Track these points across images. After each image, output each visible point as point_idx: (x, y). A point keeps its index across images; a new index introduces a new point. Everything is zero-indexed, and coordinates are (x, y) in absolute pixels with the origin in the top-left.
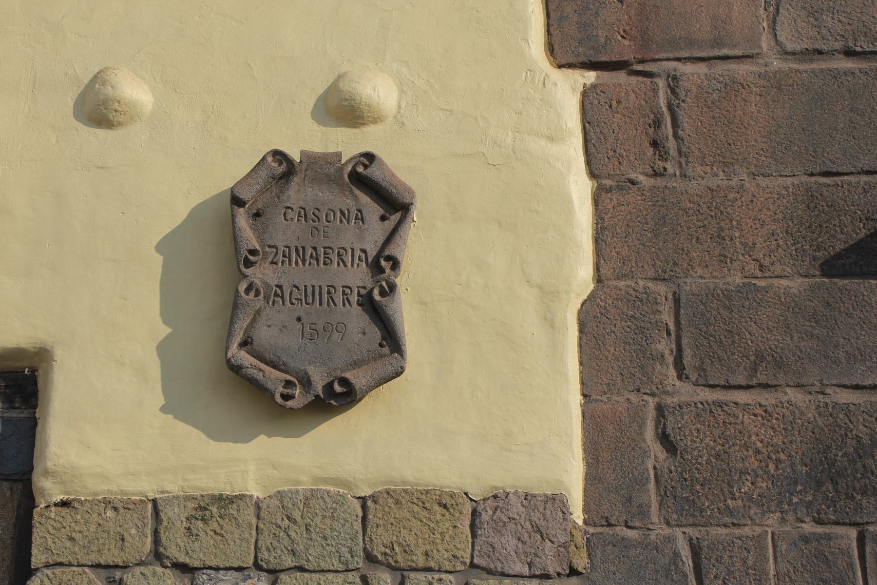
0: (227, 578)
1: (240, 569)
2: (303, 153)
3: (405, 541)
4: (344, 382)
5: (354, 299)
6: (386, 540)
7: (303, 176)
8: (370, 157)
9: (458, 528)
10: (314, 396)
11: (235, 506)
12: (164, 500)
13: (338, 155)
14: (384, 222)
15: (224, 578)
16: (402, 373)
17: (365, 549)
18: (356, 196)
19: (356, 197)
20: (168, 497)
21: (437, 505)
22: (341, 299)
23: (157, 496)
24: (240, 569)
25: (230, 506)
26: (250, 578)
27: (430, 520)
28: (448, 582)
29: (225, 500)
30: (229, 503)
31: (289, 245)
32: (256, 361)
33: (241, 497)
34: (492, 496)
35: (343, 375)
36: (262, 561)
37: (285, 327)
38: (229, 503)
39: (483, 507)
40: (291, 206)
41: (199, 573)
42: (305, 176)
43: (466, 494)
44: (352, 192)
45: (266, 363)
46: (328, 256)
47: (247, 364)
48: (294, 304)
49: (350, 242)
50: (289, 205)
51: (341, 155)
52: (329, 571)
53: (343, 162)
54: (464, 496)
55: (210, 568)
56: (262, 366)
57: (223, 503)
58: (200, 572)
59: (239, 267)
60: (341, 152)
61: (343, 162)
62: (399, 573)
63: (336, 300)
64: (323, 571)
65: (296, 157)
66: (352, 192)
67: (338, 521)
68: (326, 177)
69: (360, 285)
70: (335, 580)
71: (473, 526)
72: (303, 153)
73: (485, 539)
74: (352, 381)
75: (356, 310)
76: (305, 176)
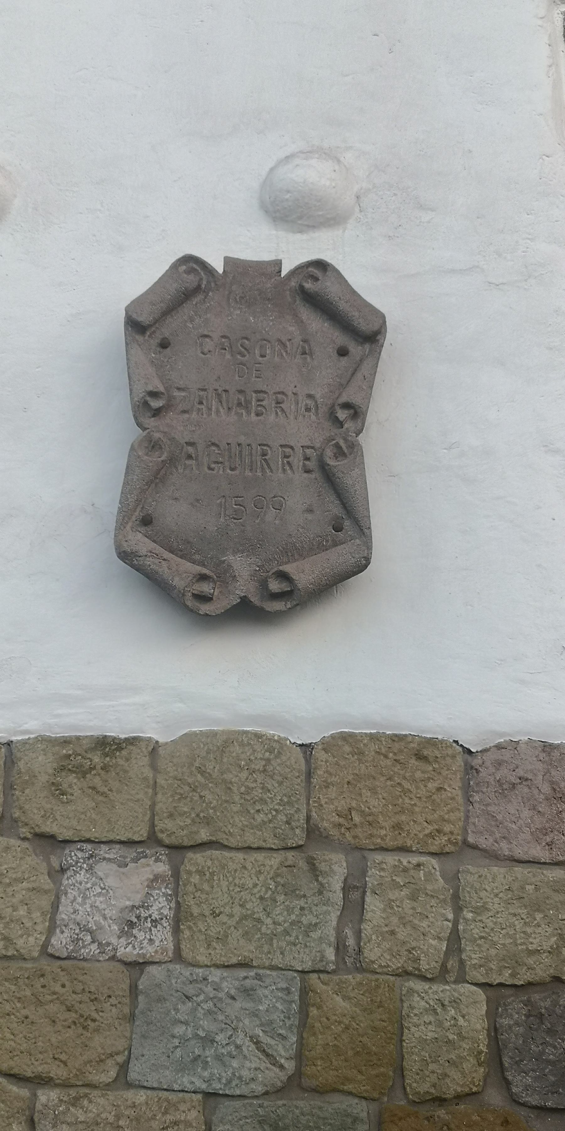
0: (112, 856)
1: (129, 843)
2: (228, 261)
3: (369, 808)
4: (283, 576)
5: (297, 461)
6: (342, 805)
7: (227, 293)
8: (321, 265)
9: (445, 790)
10: (241, 598)
11: (124, 752)
12: (25, 742)
13: (278, 263)
14: (341, 358)
15: (107, 856)
16: (366, 566)
17: (308, 818)
18: (302, 322)
19: (300, 323)
20: (29, 739)
21: (414, 758)
22: (280, 463)
23: (14, 739)
24: (129, 843)
25: (118, 754)
26: (146, 857)
27: (405, 778)
28: (431, 868)
29: (111, 745)
30: (116, 749)
31: (207, 387)
32: (158, 547)
33: (132, 741)
34: (494, 746)
35: (281, 568)
36: (162, 832)
37: (197, 500)
38: (116, 749)
39: (480, 762)
40: (210, 334)
41: (72, 849)
42: (230, 293)
43: (456, 742)
44: (296, 316)
45: (172, 552)
46: (261, 403)
47: (143, 551)
48: (213, 469)
49: (293, 385)
50: (206, 333)
51: (281, 264)
52: (259, 849)
53: (283, 273)
54: (454, 745)
55: (88, 841)
56: (167, 555)
57: (107, 750)
58: (73, 846)
59: (501, 1060)
60: (281, 261)
61: (283, 273)
62: (357, 854)
63: (272, 465)
64: (250, 848)
65: (219, 267)
66: (296, 316)
67: (272, 777)
68: (259, 295)
69: (306, 444)
70: (268, 862)
71: (467, 789)
72: (228, 261)
73: (483, 807)
74: (294, 577)
75: (299, 477)
76: (230, 293)
